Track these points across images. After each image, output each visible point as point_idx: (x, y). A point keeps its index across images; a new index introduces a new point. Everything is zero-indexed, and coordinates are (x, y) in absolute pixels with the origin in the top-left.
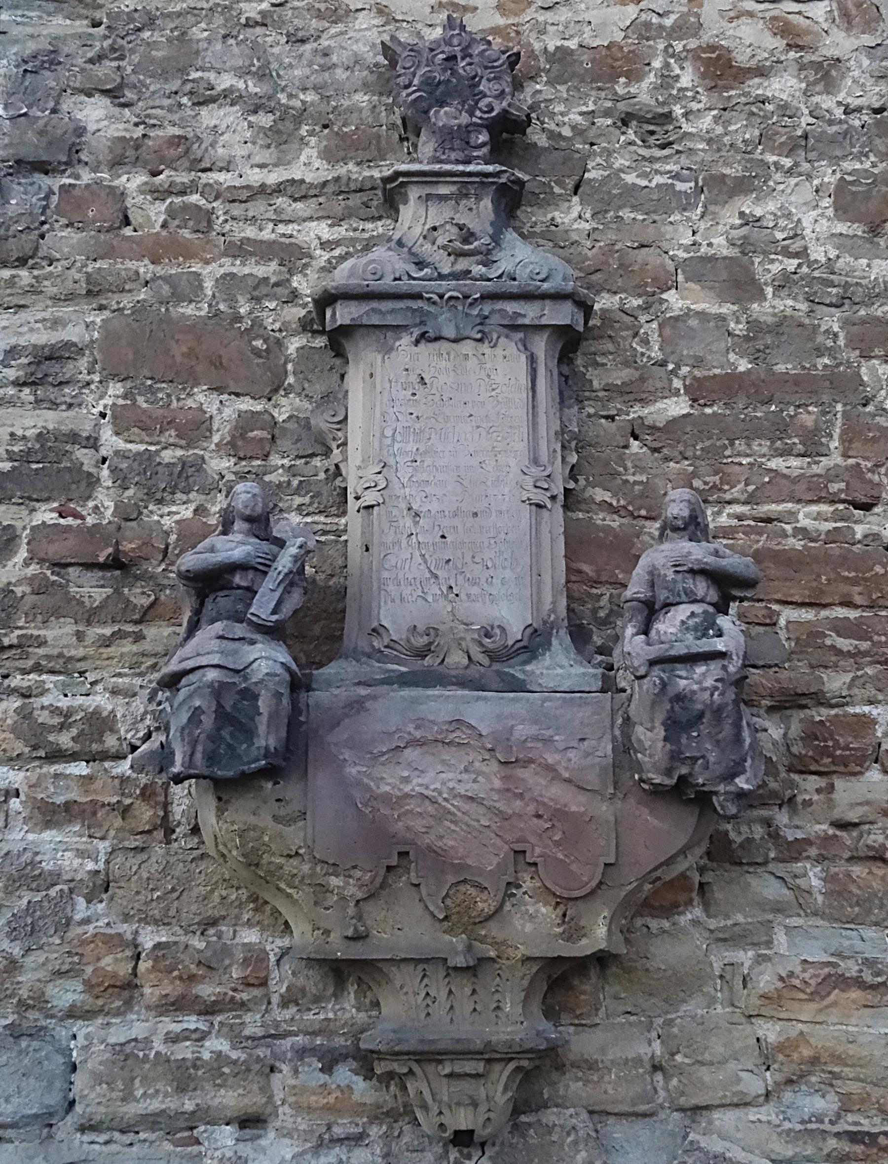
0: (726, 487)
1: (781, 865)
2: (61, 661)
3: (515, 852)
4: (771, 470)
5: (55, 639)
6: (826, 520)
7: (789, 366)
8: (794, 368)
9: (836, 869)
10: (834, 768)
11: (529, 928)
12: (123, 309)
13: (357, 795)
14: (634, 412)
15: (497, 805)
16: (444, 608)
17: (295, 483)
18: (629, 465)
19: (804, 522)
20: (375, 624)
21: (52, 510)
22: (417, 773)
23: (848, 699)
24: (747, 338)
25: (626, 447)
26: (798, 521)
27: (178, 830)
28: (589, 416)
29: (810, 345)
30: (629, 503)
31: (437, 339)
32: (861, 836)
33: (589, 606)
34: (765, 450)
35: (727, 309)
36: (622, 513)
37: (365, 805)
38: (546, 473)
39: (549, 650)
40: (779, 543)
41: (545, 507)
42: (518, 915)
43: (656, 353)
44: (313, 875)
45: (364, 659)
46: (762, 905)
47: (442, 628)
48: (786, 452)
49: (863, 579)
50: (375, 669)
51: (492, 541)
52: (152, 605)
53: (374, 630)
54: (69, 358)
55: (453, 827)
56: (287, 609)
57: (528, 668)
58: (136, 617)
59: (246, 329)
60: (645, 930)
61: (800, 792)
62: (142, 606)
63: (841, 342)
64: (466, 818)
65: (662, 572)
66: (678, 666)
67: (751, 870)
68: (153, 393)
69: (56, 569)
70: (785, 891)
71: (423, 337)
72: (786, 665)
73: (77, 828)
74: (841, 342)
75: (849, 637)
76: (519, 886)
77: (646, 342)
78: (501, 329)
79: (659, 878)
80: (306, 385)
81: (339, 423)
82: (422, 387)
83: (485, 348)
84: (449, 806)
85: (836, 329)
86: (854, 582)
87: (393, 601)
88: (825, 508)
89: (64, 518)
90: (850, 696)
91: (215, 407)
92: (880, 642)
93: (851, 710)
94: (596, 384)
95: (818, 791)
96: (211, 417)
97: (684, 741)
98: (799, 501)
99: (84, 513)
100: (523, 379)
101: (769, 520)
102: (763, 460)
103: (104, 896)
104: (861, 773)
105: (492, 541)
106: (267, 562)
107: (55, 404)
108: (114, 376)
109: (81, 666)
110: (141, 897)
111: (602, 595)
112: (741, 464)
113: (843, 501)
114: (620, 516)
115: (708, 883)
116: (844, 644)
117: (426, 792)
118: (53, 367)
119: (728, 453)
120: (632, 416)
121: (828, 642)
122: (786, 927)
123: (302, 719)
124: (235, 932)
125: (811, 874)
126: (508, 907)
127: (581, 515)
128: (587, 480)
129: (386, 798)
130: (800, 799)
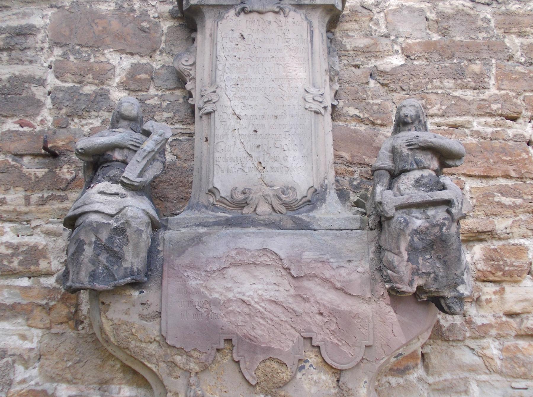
0: (429, 107)
1: (473, 341)
2: (15, 214)
3: (304, 338)
4: (455, 97)
5: (12, 200)
6: (490, 126)
7: (463, 38)
8: (466, 39)
9: (509, 343)
10: (504, 278)
11: (314, 390)
12: (64, 6)
13: (195, 299)
14: (371, 64)
15: (292, 306)
16: (255, 176)
17: (165, 104)
18: (370, 94)
19: (476, 127)
20: (211, 187)
21: (15, 123)
22: (237, 284)
23: (510, 235)
24: (437, 22)
25: (367, 83)
26: (473, 127)
27: (85, 321)
28: (345, 65)
29: (474, 26)
30: (370, 116)
31: (251, 12)
32: (522, 321)
33: (347, 178)
34: (451, 85)
35: (423, 5)
36: (366, 122)
37: (202, 307)
38: (321, 93)
39: (324, 202)
40: (464, 140)
41: (321, 113)
42: (307, 381)
43: (383, 30)
44: (166, 355)
45: (203, 210)
46: (461, 367)
47: (254, 188)
48: (464, 87)
49: (515, 161)
50: (210, 215)
51: (287, 134)
52: (74, 179)
53: (210, 191)
54: (30, 34)
55: (262, 321)
56: (149, 175)
57: (311, 214)
58: (63, 186)
59: (137, 16)
60: (387, 385)
61: (483, 294)
62: (67, 179)
63: (492, 24)
64: (271, 316)
65: (400, 150)
66: (414, 210)
67: (454, 344)
68: (79, 54)
69: (16, 158)
70: (476, 358)
71: (243, 10)
72: (471, 214)
73: (124, 301)
74: (492, 24)
75: (509, 196)
76: (306, 361)
77: (377, 24)
78: (291, 7)
79: (401, 354)
80: (173, 48)
81: (191, 65)
82: (242, 41)
83: (281, 17)
84: (259, 307)
85: (489, 16)
86: (510, 163)
87: (222, 172)
88: (490, 120)
89: (22, 127)
90: (512, 233)
91: (117, 61)
92: (528, 199)
93: (512, 241)
94: (348, 47)
95: (495, 293)
96: (115, 67)
97: (420, 261)
98: (473, 115)
99: (35, 124)
100: (306, 36)
101: (456, 127)
102: (451, 91)
103: (37, 365)
104: (520, 281)
105: (287, 134)
106: (137, 144)
107: (21, 60)
108: (57, 44)
109: (26, 217)
110: (60, 366)
111: (355, 171)
112: (437, 94)
113: (501, 115)
114: (365, 124)
115: (426, 353)
116: (507, 201)
117: (243, 298)
118: (21, 39)
119: (429, 86)
120: (370, 66)
121: (496, 199)
122: (477, 381)
123: (160, 248)
124: (120, 389)
125: (492, 346)
126: (299, 375)
127: (341, 123)
128: (344, 102)
129: (215, 302)
130: (483, 298)
